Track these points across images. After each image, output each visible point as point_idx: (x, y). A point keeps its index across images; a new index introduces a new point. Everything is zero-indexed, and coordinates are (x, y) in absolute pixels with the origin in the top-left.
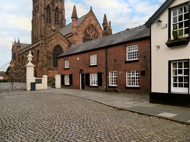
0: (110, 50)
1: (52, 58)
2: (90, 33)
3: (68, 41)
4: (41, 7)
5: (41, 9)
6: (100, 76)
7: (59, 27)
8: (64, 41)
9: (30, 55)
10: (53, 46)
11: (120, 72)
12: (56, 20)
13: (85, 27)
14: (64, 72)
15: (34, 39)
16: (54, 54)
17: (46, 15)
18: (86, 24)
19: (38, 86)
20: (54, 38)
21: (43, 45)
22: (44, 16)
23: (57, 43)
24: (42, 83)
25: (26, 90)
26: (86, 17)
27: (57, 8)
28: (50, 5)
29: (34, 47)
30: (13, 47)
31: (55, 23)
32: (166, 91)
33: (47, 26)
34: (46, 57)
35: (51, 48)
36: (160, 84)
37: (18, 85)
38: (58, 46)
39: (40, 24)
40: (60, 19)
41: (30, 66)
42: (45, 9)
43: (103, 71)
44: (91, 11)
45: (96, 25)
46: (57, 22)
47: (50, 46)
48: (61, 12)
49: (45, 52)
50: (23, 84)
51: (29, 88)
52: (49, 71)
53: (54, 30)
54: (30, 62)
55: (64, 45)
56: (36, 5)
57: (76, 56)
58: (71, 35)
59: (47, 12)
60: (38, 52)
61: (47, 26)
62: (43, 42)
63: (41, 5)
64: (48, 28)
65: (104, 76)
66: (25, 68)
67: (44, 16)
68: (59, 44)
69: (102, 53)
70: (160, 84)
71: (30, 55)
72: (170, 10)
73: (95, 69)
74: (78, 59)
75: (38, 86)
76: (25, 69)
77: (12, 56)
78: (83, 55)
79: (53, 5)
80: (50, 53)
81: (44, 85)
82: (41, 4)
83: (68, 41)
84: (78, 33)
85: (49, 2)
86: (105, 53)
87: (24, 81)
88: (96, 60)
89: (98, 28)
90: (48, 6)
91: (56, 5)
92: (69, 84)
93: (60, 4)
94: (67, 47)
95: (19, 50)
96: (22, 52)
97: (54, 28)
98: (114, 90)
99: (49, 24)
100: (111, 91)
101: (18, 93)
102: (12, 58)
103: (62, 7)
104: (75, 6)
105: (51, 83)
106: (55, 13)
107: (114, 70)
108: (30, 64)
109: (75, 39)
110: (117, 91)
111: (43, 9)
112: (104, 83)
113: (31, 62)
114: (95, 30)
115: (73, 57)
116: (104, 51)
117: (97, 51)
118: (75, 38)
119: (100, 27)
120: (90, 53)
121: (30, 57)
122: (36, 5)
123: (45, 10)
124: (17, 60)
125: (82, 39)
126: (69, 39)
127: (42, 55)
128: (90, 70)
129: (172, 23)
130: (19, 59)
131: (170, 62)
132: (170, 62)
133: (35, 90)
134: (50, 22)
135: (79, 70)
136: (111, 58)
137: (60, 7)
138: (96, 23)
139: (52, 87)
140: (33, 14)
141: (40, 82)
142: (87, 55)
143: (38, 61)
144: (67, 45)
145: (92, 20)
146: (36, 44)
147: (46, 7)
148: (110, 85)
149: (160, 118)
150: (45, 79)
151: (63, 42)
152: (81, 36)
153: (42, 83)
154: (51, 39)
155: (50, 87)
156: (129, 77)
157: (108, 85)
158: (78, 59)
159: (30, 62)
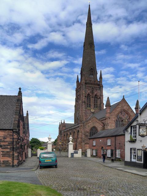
0: (117, 138)
1: (89, 135)
3: (102, 123)
4: (82, 96)
5: (83, 97)
6: (112, 151)
7: (97, 109)
8: (99, 123)
9: (71, 137)
10: (90, 127)
11: (122, 150)
12: (95, 104)
13: (117, 112)
15: (77, 118)
16: (90, 133)
17: (86, 102)
18: (119, 110)
19: (75, 155)
20: (90, 121)
21: (82, 127)
22: (85, 102)
24: (78, 153)
25: (68, 157)
26: (118, 104)
27: (96, 95)
28: (90, 94)
29: (75, 128)
30: (60, 126)
31: (95, 107)
32: (129, 161)
33: (87, 110)
34: (83, 136)
35: (88, 129)
36: (127, 159)
37: (63, 154)
38: (94, 127)
39: (82, 109)
40: (99, 103)
41: (70, 144)
42: (86, 97)
43: (114, 149)
44: (124, 99)
45: (128, 110)
46: (96, 106)
47: (87, 127)
48: (100, 98)
49: (83, 132)
50: (67, 153)
51: (70, 156)
52: (86, 145)
53: (93, 113)
54: (71, 142)
55: (99, 127)
56: (78, 94)
57: (99, 139)
58: (105, 118)
59: (87, 99)
60: (78, 131)
61: (87, 110)
62: (82, 125)
63: (83, 95)
64: (88, 111)
65: (114, 151)
66: (68, 144)
67: (85, 102)
68: (95, 125)
69: (113, 139)
70: (127, 159)
71: (71, 137)
72: (131, 127)
73: (110, 147)
74: (101, 141)
75: (75, 155)
76: (68, 146)
77: (59, 132)
78: (103, 139)
79: (93, 93)
80: (87, 132)
81: (79, 155)
82: (82, 93)
83: (102, 123)
84: (111, 117)
85: (89, 92)
87: (67, 151)
89: (129, 112)
90: (89, 94)
91: (95, 93)
92: (110, 156)
93: (99, 91)
95: (64, 128)
96: (66, 130)
97: (92, 111)
98: (119, 160)
99: (89, 108)
100: (118, 160)
101: (63, 158)
102: (59, 134)
103: (100, 94)
104: (108, 97)
105: (84, 153)
106: (95, 99)
107: (119, 149)
108: (71, 142)
109: (108, 122)
110: (120, 160)
111: (84, 97)
112: (114, 155)
113: (72, 141)
114: (127, 114)
115: (98, 139)
116: (114, 138)
118: (108, 121)
119: (132, 111)
120: (107, 138)
121: (71, 139)
122: (78, 94)
123: (86, 98)
124: (63, 135)
125: (114, 121)
126: (103, 122)
127: (81, 134)
128: (107, 148)
129: (15, 171)
130: (64, 135)
131: (131, 149)
133: (73, 157)
134: (90, 106)
136: (118, 142)
137: (98, 94)
138: (129, 108)
139: (85, 156)
140: (76, 101)
141: (77, 153)
142: (105, 139)
143: (78, 138)
144: (102, 127)
145: (125, 106)
146: (77, 126)
147: (86, 95)
148: (117, 157)
149: (118, 169)
150: (80, 151)
152: (114, 119)
153: (78, 153)
154: (89, 122)
155: (83, 156)
156: (134, 154)
157: (116, 157)
158: (101, 141)
159: (71, 142)
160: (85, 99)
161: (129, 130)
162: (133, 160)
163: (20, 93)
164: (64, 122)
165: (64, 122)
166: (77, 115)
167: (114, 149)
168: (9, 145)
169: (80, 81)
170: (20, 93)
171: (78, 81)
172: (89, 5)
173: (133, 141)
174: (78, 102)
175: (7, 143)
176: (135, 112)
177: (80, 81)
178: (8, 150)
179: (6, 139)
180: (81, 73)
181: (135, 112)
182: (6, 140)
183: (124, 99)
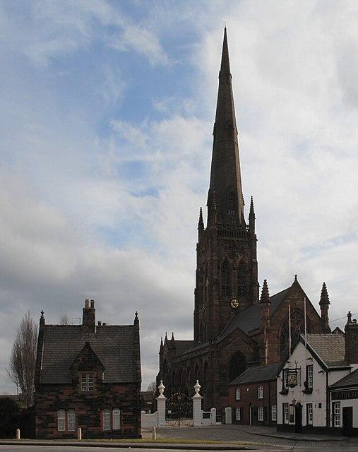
4: (212, 266)
41: (196, 398)
43: (267, 405)
44: (296, 284)
67: (217, 283)
71: (198, 385)
105: (220, 416)
108: (162, 396)
144: (252, 351)
160: (218, 273)
161: (281, 374)
162: (287, 422)
163: (137, 321)
164: (173, 337)
165: (173, 337)
166: (201, 316)
167: (267, 405)
168: (131, 407)
169: (205, 227)
170: (137, 321)
171: (201, 224)
172: (225, 29)
173: (285, 392)
174: (202, 281)
175: (129, 404)
176: (319, 313)
177: (205, 227)
178: (131, 413)
179: (128, 397)
180: (209, 204)
181: (319, 313)
182: (128, 399)
183: (296, 284)
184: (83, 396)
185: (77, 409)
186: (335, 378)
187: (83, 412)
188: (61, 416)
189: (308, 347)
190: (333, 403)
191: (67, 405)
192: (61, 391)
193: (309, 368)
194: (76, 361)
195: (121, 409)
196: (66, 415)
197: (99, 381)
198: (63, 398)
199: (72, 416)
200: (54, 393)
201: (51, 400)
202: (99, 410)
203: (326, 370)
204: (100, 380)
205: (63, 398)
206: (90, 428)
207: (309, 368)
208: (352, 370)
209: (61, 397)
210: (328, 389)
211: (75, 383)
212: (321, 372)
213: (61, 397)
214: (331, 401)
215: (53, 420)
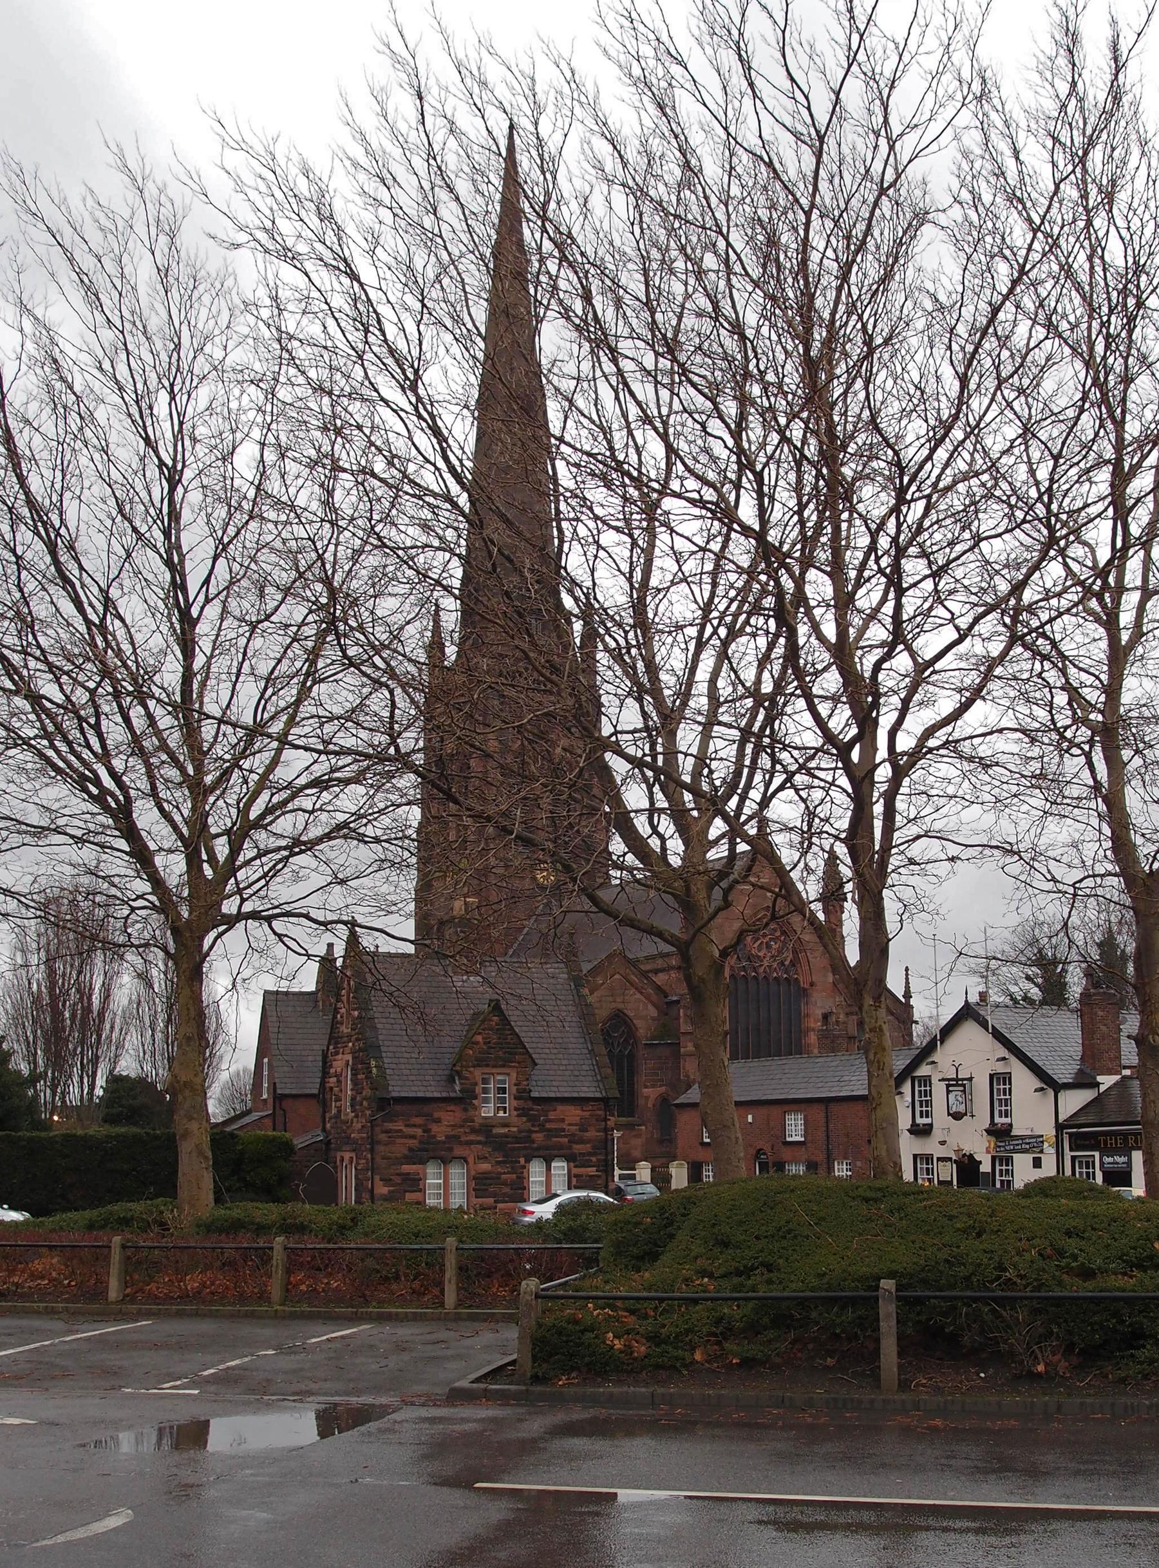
2: (759, 948)
11: (859, 1164)
14: (701, 1155)
23: (614, 1005)
68: (621, 1006)
69: (818, 1113)
73: (802, 1153)
78: (764, 1111)
86: (823, 1115)
88: (801, 1127)
94: (653, 1019)
117: (803, 1106)
120: (786, 1108)
128: (786, 1154)
131: (915, 1156)
132: (915, 1156)
135: (753, 1151)
142: (776, 1111)
144: (653, 1012)
151: (638, 996)
175: (587, 1148)
177: (451, 651)
184: (486, 1128)
185: (471, 1160)
186: (1073, 1102)
187: (485, 1166)
188: (433, 1177)
189: (998, 1035)
190: (1073, 1158)
191: (451, 1149)
192: (436, 1115)
193: (1000, 1080)
194: (470, 1043)
195: (570, 1158)
196: (549, 1169)
197: (523, 1094)
198: (440, 1132)
199: (458, 1176)
200: (419, 1120)
201: (413, 1137)
202: (522, 1160)
203: (1049, 1083)
204: (524, 1091)
205: (440, 1132)
206: (500, 1205)
207: (1000, 1080)
208: (1102, 1088)
209: (435, 1128)
210: (1059, 1127)
211: (467, 1099)
212: (1042, 1089)
213: (435, 1128)
214: (1068, 1155)
215: (415, 1183)
